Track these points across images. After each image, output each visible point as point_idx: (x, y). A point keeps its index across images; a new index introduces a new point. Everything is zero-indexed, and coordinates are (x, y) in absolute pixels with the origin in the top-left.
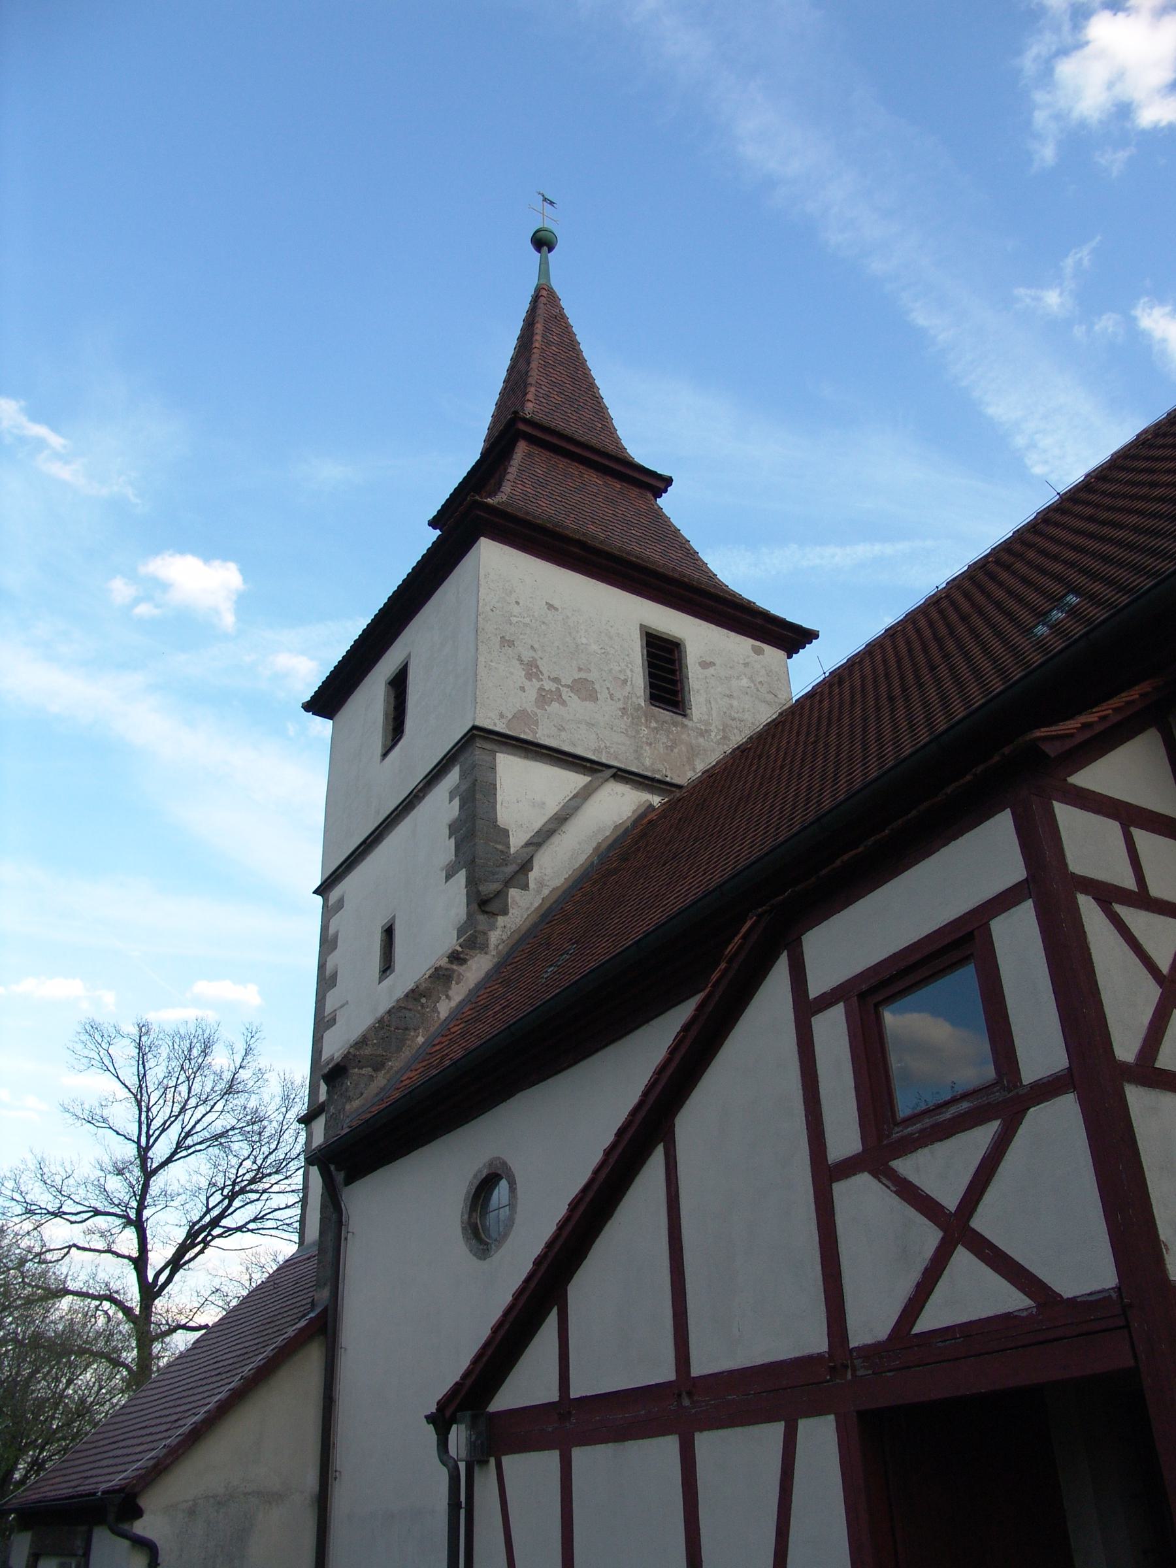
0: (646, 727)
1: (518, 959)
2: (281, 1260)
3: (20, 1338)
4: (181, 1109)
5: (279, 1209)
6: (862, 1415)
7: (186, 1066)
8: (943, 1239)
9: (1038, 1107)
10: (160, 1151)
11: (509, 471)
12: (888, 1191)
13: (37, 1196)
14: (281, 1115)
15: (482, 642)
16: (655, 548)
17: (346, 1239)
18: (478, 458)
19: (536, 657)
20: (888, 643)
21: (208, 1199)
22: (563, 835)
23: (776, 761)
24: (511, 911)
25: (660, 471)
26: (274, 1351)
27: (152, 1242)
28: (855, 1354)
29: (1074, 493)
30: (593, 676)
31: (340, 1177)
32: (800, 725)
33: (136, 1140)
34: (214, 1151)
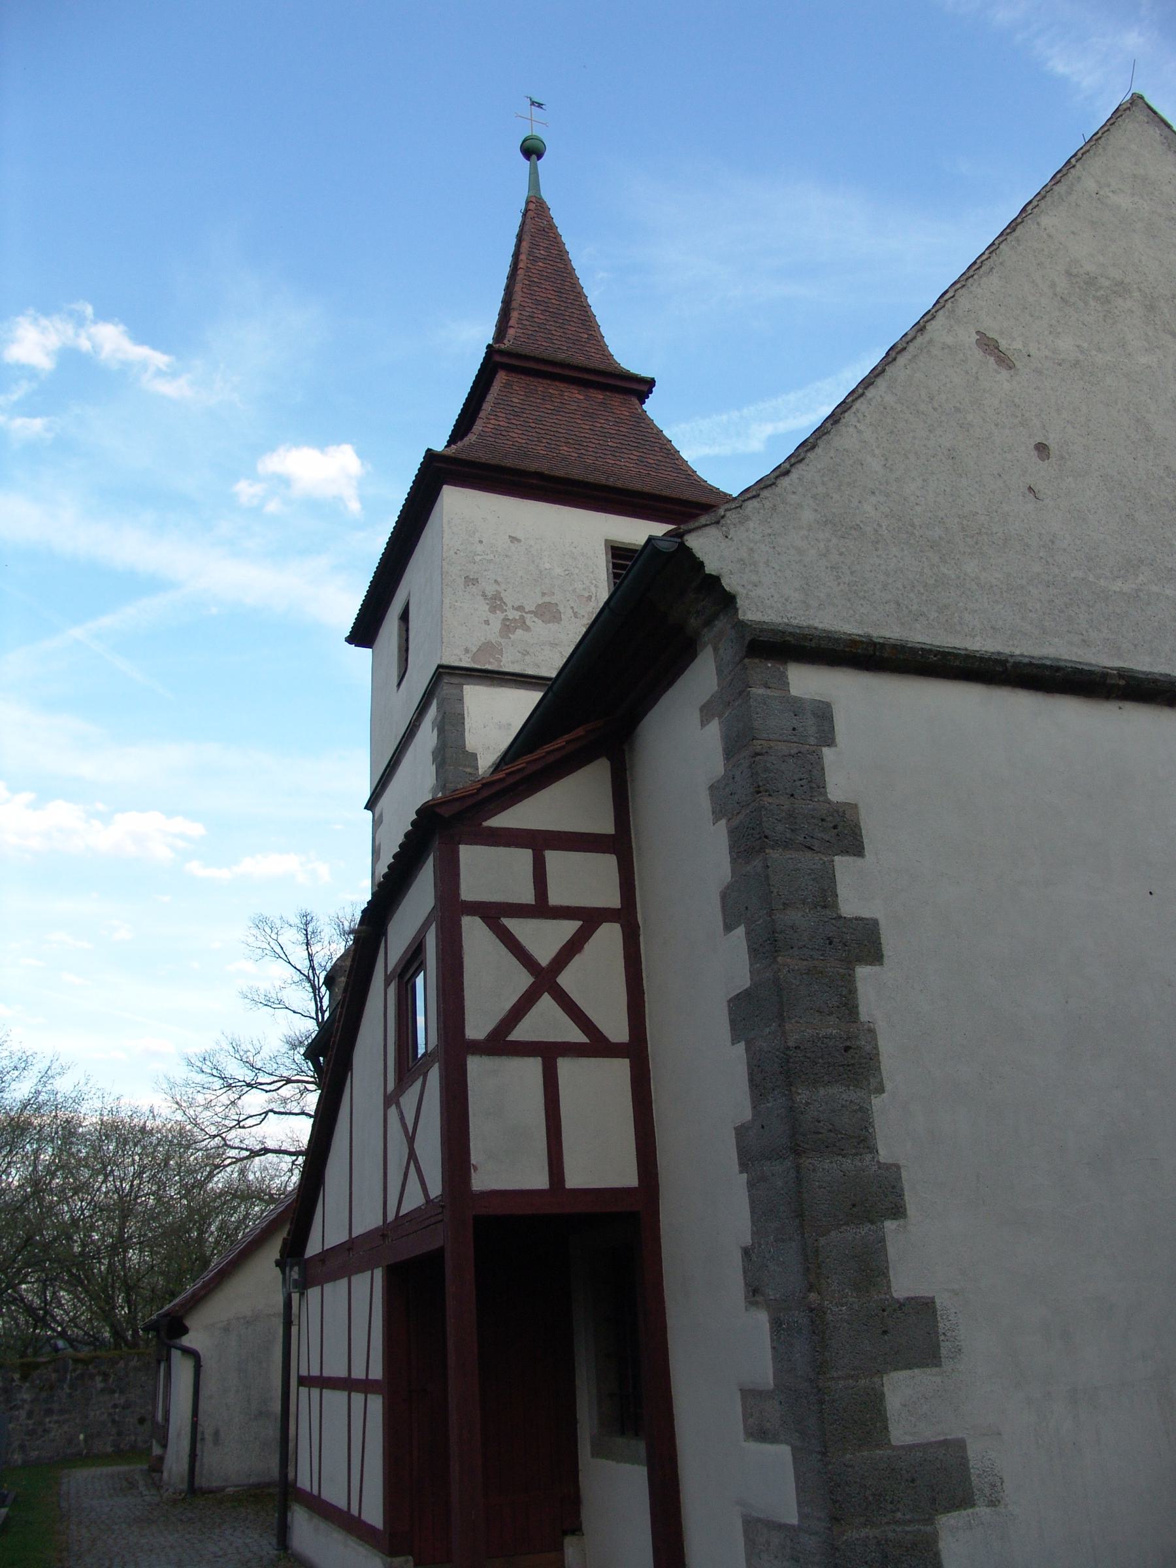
19: (499, 589)
25: (644, 374)
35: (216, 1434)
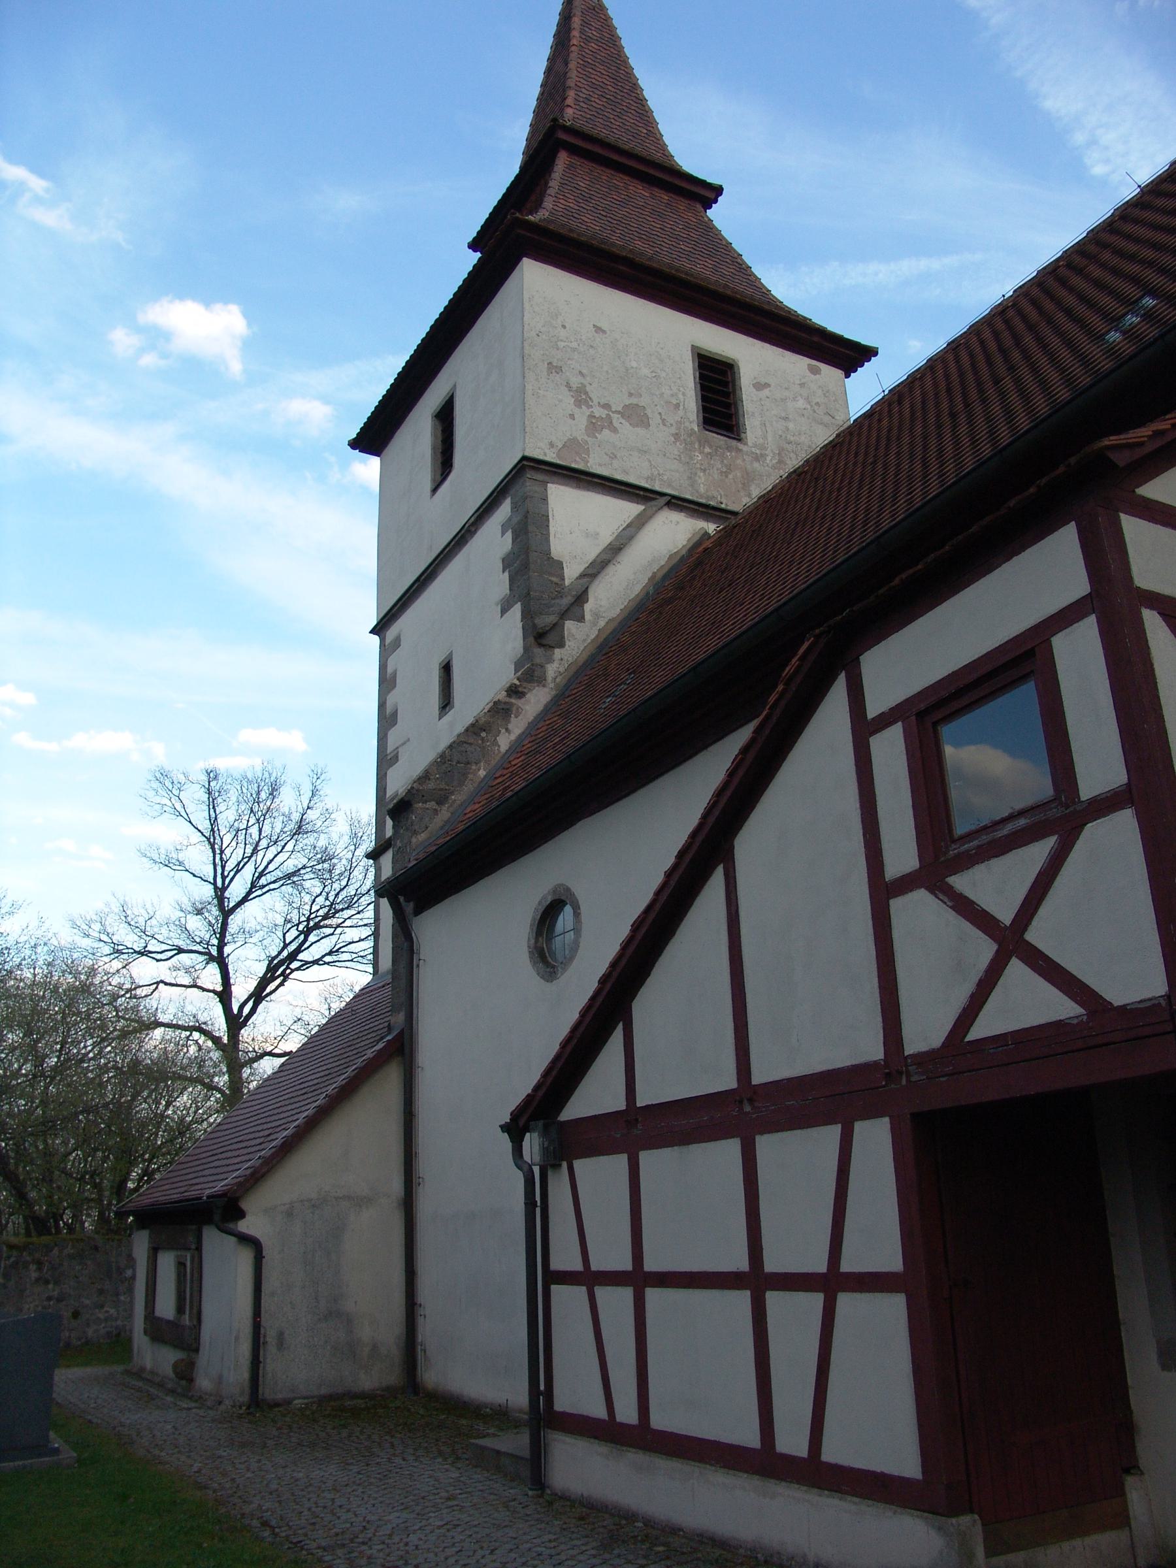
0: (700, 453)
1: (576, 691)
2: (357, 989)
3: (120, 1066)
4: (254, 850)
5: (353, 942)
6: (915, 1116)
7: (256, 809)
8: (997, 951)
9: (1095, 823)
10: (236, 891)
11: (550, 185)
12: (945, 906)
13: (123, 937)
14: (350, 852)
15: (529, 369)
16: (706, 264)
17: (418, 966)
18: (517, 172)
20: (951, 357)
21: (284, 935)
22: (618, 565)
23: (833, 483)
24: (567, 643)
25: (710, 180)
26: (356, 1071)
27: (234, 977)
28: (909, 1061)
29: (1157, 184)
30: (644, 401)
31: (409, 908)
32: (858, 446)
33: (212, 881)
34: (288, 889)
35: (281, 1335)
